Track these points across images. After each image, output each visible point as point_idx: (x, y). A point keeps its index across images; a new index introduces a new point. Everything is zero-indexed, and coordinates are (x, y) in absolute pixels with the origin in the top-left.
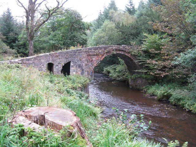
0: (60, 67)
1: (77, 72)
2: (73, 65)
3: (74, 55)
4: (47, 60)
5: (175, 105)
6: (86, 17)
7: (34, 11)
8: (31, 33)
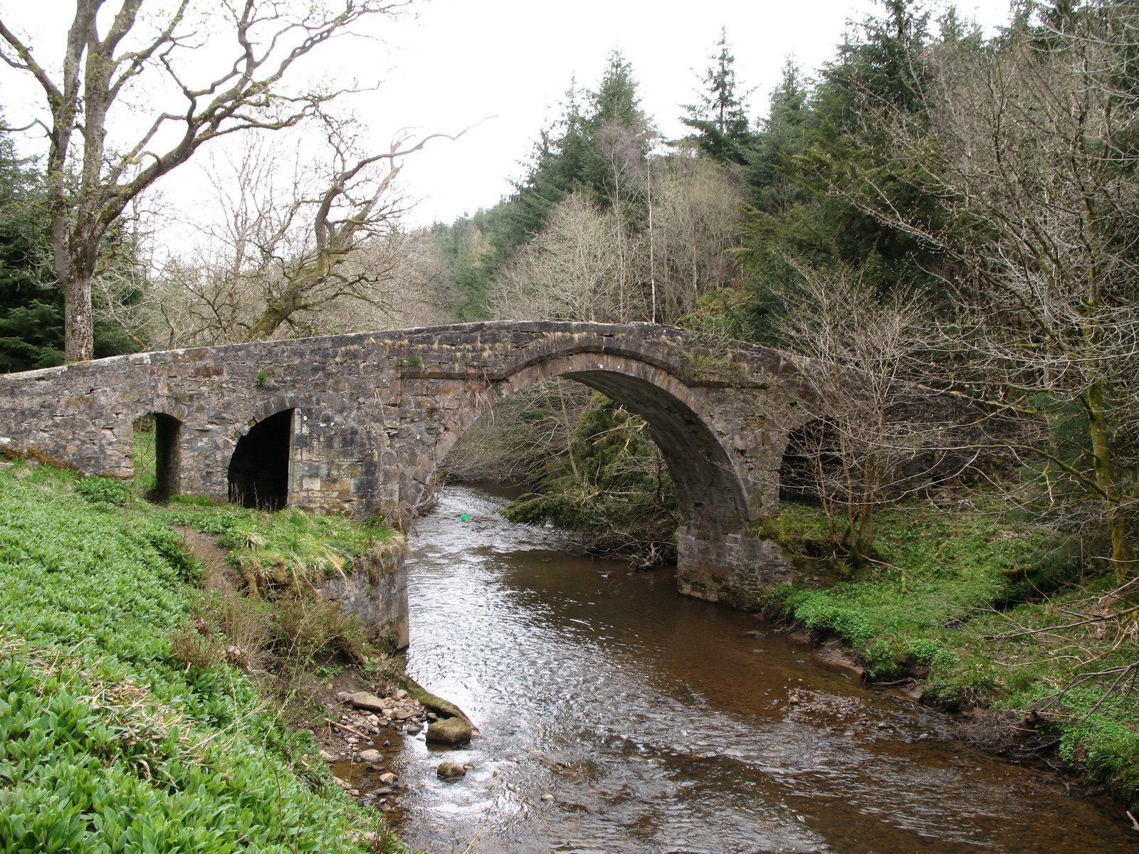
0: (220, 442)
1: (330, 480)
2: (305, 431)
3: (315, 370)
4: (135, 395)
5: (265, 84)
6: (420, 147)
7: (100, 97)
8: (78, 233)
